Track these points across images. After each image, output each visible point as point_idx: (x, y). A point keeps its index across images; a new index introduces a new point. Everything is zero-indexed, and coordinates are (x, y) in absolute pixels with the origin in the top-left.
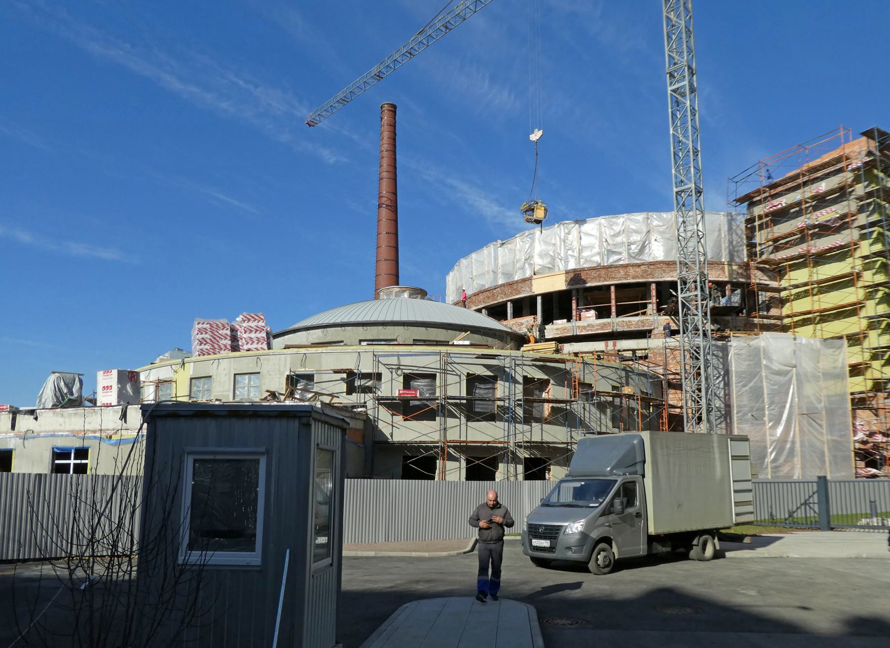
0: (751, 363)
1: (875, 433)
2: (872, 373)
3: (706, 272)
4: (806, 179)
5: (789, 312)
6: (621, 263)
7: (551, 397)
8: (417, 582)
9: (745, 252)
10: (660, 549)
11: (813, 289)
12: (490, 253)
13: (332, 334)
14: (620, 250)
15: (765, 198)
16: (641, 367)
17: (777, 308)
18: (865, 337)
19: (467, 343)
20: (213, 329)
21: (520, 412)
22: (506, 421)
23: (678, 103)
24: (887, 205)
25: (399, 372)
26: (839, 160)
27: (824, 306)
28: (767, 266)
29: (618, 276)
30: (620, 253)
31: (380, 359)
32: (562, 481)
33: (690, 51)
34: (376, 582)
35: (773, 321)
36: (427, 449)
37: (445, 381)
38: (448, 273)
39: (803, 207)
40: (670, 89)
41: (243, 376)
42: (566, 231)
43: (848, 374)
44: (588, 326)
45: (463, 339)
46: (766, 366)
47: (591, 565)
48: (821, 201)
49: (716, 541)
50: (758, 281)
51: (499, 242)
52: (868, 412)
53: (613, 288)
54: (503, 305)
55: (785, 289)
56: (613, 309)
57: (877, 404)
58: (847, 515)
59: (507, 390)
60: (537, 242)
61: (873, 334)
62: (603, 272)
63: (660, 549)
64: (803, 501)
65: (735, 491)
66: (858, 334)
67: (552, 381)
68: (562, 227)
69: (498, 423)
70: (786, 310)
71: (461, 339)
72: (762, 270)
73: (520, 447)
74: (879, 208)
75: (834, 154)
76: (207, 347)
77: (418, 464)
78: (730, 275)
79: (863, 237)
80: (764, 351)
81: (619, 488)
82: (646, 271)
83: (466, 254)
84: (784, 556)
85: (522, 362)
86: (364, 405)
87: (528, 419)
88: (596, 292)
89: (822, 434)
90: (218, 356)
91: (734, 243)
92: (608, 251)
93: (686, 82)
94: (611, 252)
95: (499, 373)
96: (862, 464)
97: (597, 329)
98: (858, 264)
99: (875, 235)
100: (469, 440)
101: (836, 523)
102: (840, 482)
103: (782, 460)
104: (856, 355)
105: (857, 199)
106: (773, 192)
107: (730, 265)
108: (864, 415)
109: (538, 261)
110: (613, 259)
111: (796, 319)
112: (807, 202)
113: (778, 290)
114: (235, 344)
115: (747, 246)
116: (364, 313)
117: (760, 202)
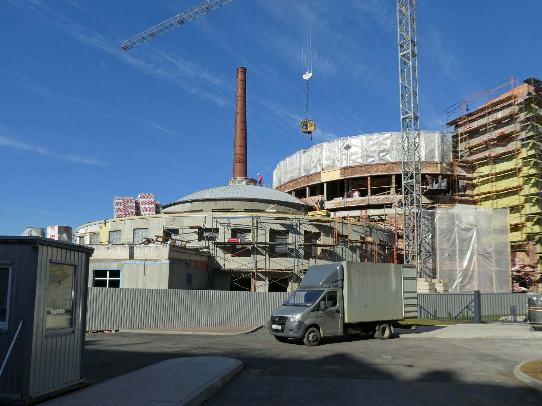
0: (449, 223)
1: (526, 266)
2: (526, 230)
3: (420, 168)
4: (490, 110)
5: (477, 193)
6: (375, 163)
7: (322, 243)
8: (196, 348)
9: (451, 155)
10: (352, 331)
11: (492, 178)
12: (297, 157)
13: (197, 206)
14: (374, 155)
15: (465, 123)
16: (381, 225)
17: (470, 190)
18: (523, 208)
19: (274, 211)
20: (125, 203)
21: (302, 252)
22: (293, 257)
23: (405, 63)
24: (540, 126)
25: (229, 228)
26: (510, 98)
27: (499, 188)
28: (465, 164)
29: (372, 171)
30: (374, 157)
31: (218, 220)
32: (296, 291)
33: (413, 31)
34: (173, 348)
35: (467, 198)
36: (245, 273)
37: (257, 233)
38: (274, 170)
39: (488, 127)
40: (400, 54)
41: (138, 230)
42: (342, 144)
43: (509, 230)
44: (354, 201)
45: (272, 209)
46: (457, 225)
47: (305, 340)
48: (499, 124)
49: (392, 328)
50: (458, 174)
51: (302, 150)
52: (523, 253)
53: (369, 178)
54: (304, 189)
55: (475, 178)
56: (369, 191)
57: (529, 248)
58: (496, 315)
59: (294, 239)
60: (324, 150)
61: (527, 206)
62: (363, 168)
63: (352, 331)
64: (466, 306)
65: (405, 298)
66: (518, 206)
67: (322, 234)
68: (339, 141)
69: (289, 259)
70: (476, 191)
71: (271, 209)
72: (461, 167)
73: (301, 272)
74: (533, 128)
75: (507, 95)
76: (121, 213)
77: (241, 282)
78: (441, 170)
79: (523, 146)
80: (457, 216)
81: (325, 295)
82: (389, 168)
83: (283, 158)
84: (435, 337)
85: (304, 222)
86: (208, 248)
87: (308, 256)
88: (360, 181)
89: (491, 266)
90: (128, 218)
91: (445, 150)
92: (367, 155)
93: (410, 51)
94: (368, 156)
95: (290, 229)
96: (517, 284)
97: (359, 203)
98: (520, 163)
99: (530, 145)
100: (271, 268)
101: (484, 319)
102: (487, 294)
103: (466, 282)
104: (515, 219)
105: (520, 122)
106: (470, 118)
107: (441, 163)
108: (520, 255)
109: (325, 162)
110: (370, 160)
111: (482, 197)
112: (490, 125)
113: (471, 179)
114: (138, 211)
115: (453, 152)
116: (219, 193)
117: (461, 125)
